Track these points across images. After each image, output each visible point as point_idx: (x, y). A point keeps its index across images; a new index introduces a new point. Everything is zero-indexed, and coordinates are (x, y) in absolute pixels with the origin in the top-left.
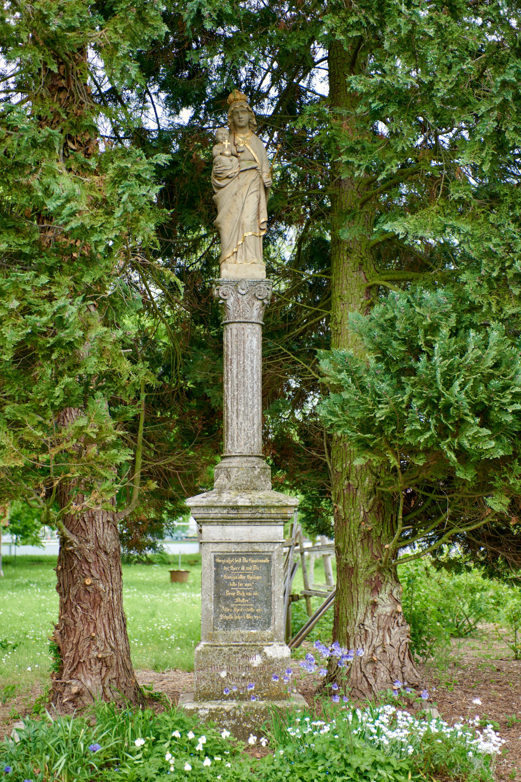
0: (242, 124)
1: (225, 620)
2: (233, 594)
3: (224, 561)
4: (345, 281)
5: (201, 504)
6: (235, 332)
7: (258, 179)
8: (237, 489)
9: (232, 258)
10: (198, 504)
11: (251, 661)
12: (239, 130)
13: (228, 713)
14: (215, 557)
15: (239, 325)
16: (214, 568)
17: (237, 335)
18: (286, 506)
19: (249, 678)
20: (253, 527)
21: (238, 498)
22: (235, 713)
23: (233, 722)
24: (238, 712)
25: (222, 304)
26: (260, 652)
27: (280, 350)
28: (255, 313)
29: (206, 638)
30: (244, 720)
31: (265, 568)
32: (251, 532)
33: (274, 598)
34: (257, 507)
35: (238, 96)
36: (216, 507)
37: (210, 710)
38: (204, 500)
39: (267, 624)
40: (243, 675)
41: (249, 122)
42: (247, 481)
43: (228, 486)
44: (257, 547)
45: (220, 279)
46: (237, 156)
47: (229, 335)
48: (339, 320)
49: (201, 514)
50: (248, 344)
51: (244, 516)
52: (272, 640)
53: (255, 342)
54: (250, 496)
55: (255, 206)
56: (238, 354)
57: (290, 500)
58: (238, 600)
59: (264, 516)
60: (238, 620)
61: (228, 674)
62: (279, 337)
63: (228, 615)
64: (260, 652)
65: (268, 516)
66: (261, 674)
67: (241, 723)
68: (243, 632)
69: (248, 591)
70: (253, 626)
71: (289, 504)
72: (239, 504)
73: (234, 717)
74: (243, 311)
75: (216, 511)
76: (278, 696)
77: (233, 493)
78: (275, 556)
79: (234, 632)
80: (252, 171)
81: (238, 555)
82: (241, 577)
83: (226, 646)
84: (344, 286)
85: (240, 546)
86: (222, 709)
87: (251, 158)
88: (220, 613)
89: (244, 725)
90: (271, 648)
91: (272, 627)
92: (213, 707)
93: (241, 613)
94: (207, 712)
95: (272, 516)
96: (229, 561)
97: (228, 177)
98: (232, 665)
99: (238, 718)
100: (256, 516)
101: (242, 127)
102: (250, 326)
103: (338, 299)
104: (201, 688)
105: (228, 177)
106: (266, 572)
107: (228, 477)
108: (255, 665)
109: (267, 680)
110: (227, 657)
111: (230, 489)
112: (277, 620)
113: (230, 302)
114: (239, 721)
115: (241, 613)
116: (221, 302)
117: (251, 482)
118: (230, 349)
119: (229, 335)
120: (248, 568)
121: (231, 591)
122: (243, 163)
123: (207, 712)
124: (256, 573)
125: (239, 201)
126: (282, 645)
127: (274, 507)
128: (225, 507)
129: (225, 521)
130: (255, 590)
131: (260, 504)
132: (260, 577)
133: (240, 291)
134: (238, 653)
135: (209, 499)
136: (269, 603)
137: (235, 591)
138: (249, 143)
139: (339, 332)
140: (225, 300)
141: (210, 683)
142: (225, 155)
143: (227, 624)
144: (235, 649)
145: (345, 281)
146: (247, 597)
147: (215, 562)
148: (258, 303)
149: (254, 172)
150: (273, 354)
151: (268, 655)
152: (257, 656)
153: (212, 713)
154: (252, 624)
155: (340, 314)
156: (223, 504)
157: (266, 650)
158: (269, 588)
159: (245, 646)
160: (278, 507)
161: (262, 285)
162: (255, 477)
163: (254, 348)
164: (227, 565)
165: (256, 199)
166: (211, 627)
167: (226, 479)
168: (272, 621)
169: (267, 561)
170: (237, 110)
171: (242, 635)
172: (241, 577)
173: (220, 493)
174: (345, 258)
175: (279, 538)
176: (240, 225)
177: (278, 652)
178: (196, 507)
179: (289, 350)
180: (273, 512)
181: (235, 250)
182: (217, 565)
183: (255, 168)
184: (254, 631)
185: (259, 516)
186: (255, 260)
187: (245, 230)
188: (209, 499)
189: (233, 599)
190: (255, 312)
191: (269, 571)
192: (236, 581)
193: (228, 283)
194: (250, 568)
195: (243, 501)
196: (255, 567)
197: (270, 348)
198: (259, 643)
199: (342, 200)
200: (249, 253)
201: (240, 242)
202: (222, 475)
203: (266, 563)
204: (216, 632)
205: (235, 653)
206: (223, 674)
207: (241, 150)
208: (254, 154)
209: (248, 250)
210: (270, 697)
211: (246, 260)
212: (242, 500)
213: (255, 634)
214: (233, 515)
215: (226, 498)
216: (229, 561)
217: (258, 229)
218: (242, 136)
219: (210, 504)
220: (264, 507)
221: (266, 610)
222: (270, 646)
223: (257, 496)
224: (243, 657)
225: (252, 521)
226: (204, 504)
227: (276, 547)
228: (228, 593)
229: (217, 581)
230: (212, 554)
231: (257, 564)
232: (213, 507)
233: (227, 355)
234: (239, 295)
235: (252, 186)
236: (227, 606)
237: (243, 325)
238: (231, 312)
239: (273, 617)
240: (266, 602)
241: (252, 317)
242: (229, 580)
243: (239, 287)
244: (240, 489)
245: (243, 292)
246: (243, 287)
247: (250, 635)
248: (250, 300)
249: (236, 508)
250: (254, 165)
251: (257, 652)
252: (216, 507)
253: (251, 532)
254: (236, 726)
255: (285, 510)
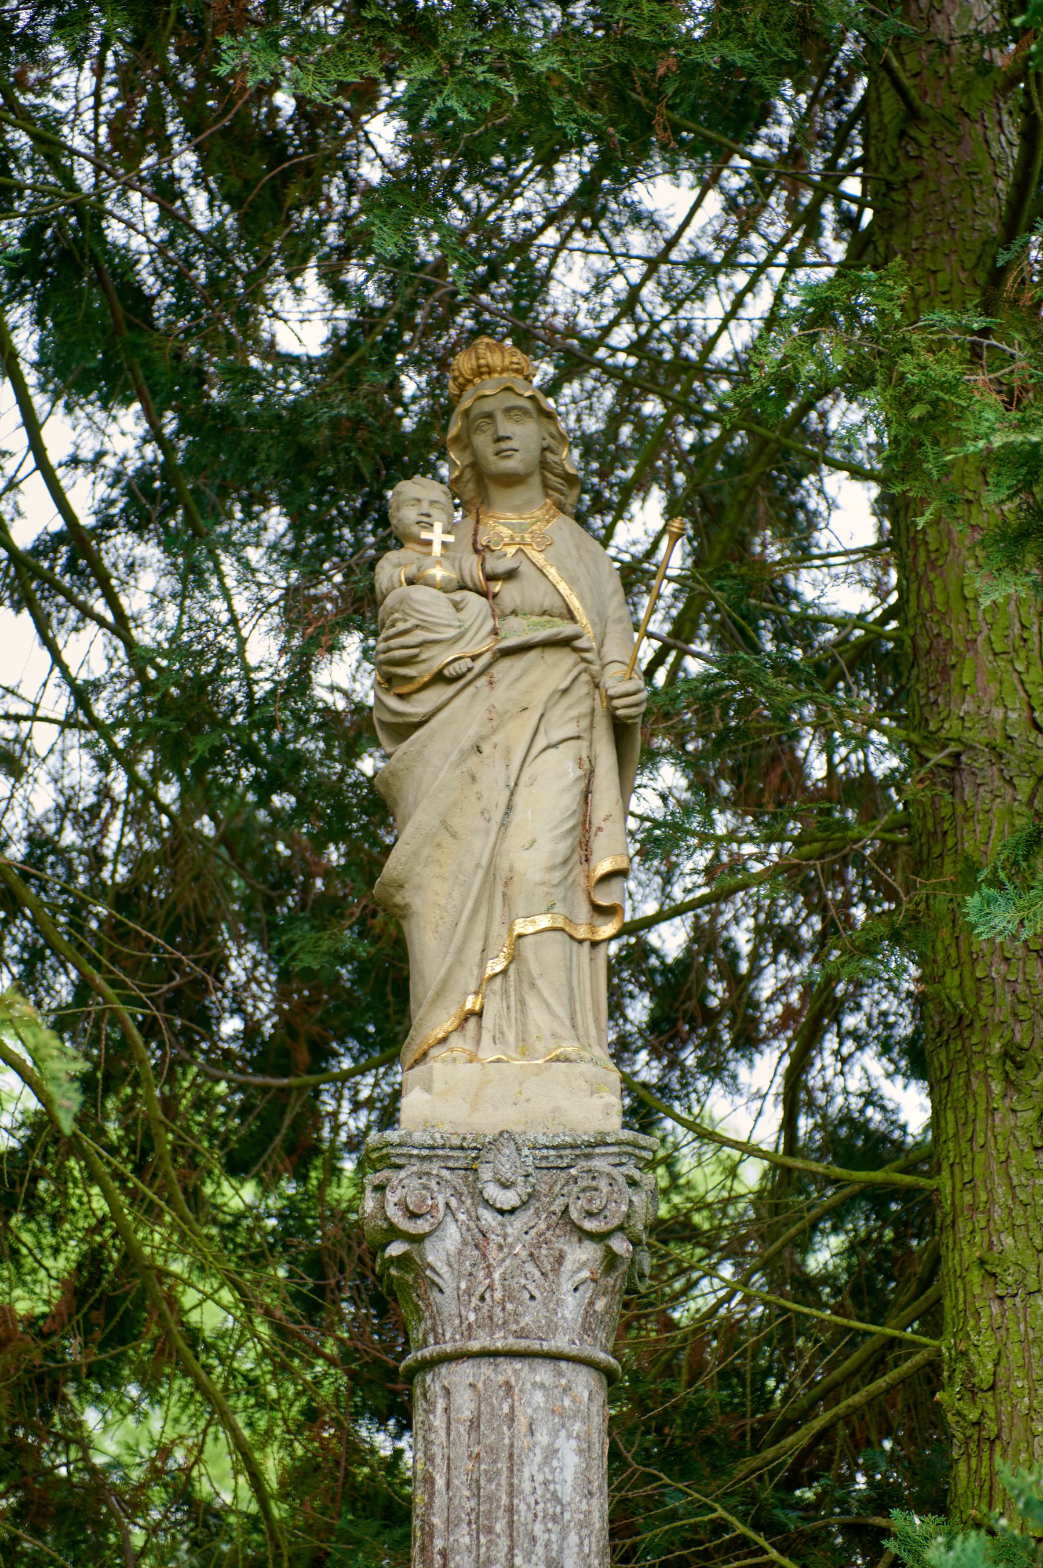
0: (512, 464)
4: (1001, 1192)
6: (465, 1404)
7: (582, 689)
9: (455, 1041)
12: (497, 495)
15: (486, 1368)
17: (474, 1424)
25: (404, 1261)
27: (720, 1527)
28: (571, 1307)
35: (495, 359)
41: (544, 465)
45: (392, 1135)
46: (484, 594)
47: (438, 1421)
48: (984, 1374)
50: (531, 1468)
53: (570, 1461)
55: (570, 800)
56: (481, 1527)
62: (717, 1470)
74: (509, 1296)
80: (553, 655)
84: (998, 1214)
87: (550, 602)
97: (440, 678)
101: (511, 480)
102: (543, 1373)
103: (975, 1276)
105: (440, 678)
113: (442, 1252)
116: (396, 1249)
118: (440, 1501)
119: (438, 1421)
122: (513, 621)
125: (493, 777)
133: (492, 1191)
138: (546, 545)
139: (991, 1428)
140: (417, 1239)
142: (430, 583)
145: (1001, 1192)
148: (581, 1257)
149: (564, 662)
150: (686, 1544)
155: (987, 1343)
161: (600, 1164)
163: (567, 1492)
165: (573, 772)
170: (487, 406)
174: (997, 1088)
176: (496, 883)
179: (756, 1527)
181: (471, 1003)
183: (566, 643)
186: (569, 1048)
187: (520, 907)
190: (569, 1302)
193: (431, 1152)
197: (673, 1516)
199: (968, 846)
200: (537, 1015)
201: (496, 966)
207: (501, 566)
208: (563, 587)
209: (532, 1002)
211: (524, 1047)
217: (584, 911)
218: (513, 518)
233: (429, 1534)
234: (488, 1217)
235: (556, 714)
237: (509, 1369)
238: (446, 1302)
241: (552, 1328)
243: (486, 1173)
245: (508, 1199)
246: (506, 1171)
248: (542, 1240)
250: (567, 629)
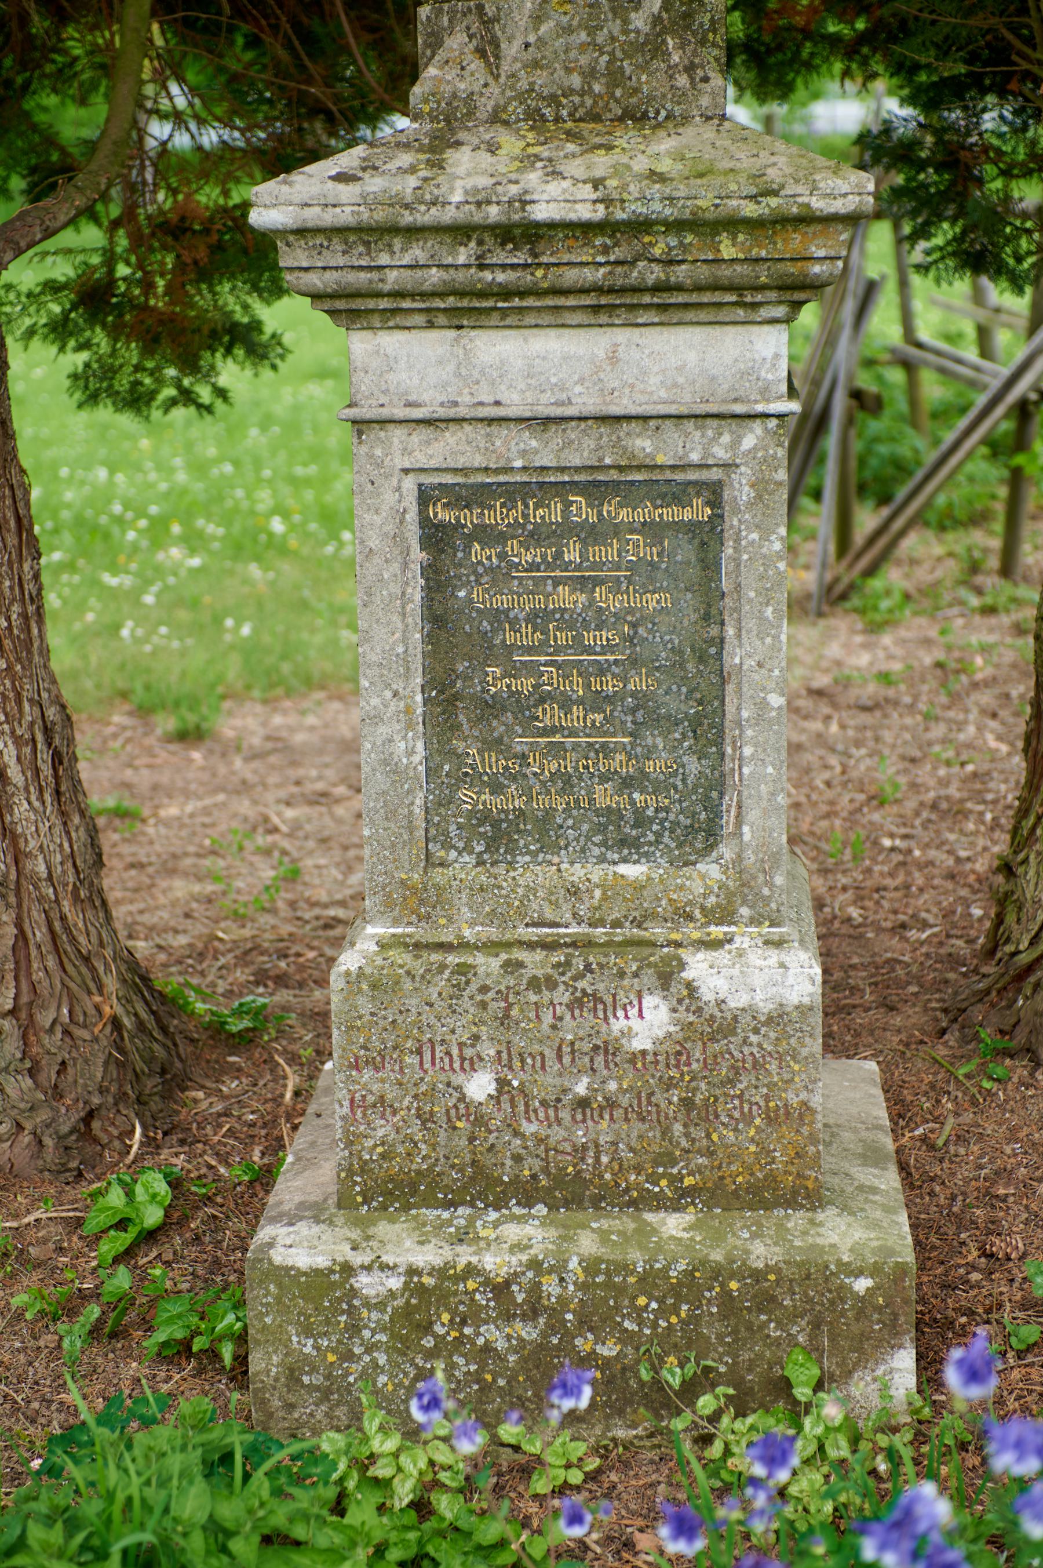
1: (485, 817)
2: (526, 685)
3: (469, 518)
5: (329, 218)
8: (535, 118)
10: (313, 216)
11: (618, 1025)
13: (501, 1289)
14: (425, 497)
16: (418, 556)
18: (806, 219)
19: (611, 1104)
20: (622, 336)
21: (533, 177)
22: (536, 1287)
23: (528, 1332)
24: (550, 1286)
26: (667, 976)
29: (389, 904)
30: (585, 1323)
31: (686, 552)
32: (613, 359)
33: (740, 708)
34: (640, 226)
36: (414, 232)
37: (412, 1271)
38: (346, 192)
39: (703, 832)
40: (581, 1089)
42: (590, 74)
43: (485, 106)
44: (643, 444)
49: (336, 265)
51: (571, 276)
52: (725, 915)
54: (601, 163)
57: (829, 182)
58: (549, 715)
59: (681, 273)
60: (549, 813)
61: (502, 1083)
63: (497, 788)
64: (667, 976)
65: (703, 273)
66: (669, 1085)
67: (568, 1336)
68: (577, 872)
69: (602, 670)
70: (629, 847)
71: (818, 204)
72: (541, 213)
73: (533, 1310)
75: (417, 253)
76: (755, 1190)
77: (510, 144)
78: (741, 490)
79: (532, 875)
81: (542, 487)
82: (566, 597)
83: (492, 947)
85: (555, 437)
86: (470, 1271)
88: (461, 779)
89: (584, 1344)
90: (721, 956)
91: (726, 851)
92: (428, 1256)
93: (566, 782)
94: (395, 1283)
95: (725, 272)
96: (495, 516)
98: (519, 1043)
99: (555, 1313)
100: (634, 268)
104: (369, 1148)
106: (693, 572)
107: (488, 50)
108: (638, 1044)
109: (698, 1112)
110: (497, 1007)
111: (496, 118)
112: (753, 815)
114: (556, 1324)
115: (566, 782)
117: (615, 77)
120: (596, 553)
121: (513, 671)
123: (395, 1283)
124: (643, 575)
126: (778, 944)
127: (733, 224)
128: (460, 232)
129: (466, 307)
130: (634, 662)
131: (657, 208)
132: (665, 600)
134: (551, 984)
135: (374, 184)
136: (708, 729)
137: (532, 669)
141: (415, 1129)
143: (498, 837)
144: (535, 962)
146: (597, 701)
147: (425, 522)
151: (707, 994)
152: (649, 1001)
153: (422, 1290)
154: (624, 836)
156: (448, 215)
157: (698, 966)
158: (710, 653)
159: (589, 944)
160: (755, 225)
162: (633, 49)
164: (484, 534)
166: (417, 850)
167: (476, 65)
168: (728, 820)
169: (697, 511)
171: (574, 891)
172: (566, 597)
173: (438, 146)
175: (765, 394)
177: (758, 980)
178: (301, 232)
180: (727, 250)
182: (436, 538)
184: (631, 871)
185: (655, 274)
188: (374, 184)
189: (523, 708)
191: (710, 565)
192: (538, 619)
194: (612, 554)
195: (557, 196)
196: (639, 548)
198: (657, 931)
202: (456, 42)
203: (692, 528)
204: (439, 876)
205: (534, 984)
206: (480, 1086)
210: (716, 1196)
212: (555, 188)
213: (639, 887)
214: (514, 268)
215: (472, 176)
216: (495, 516)
219: (380, 216)
220: (678, 226)
221: (693, 766)
222: (715, 944)
223: (641, 164)
224: (576, 1004)
225: (613, 303)
226: (345, 216)
227: (749, 442)
228: (496, 680)
229: (439, 618)
230: (409, 484)
231: (645, 528)
232: (393, 230)
236: (496, 745)
239: (730, 800)
240: (695, 723)
242: (499, 616)
244: (560, 117)
247: (613, 889)
249: (525, 235)
251: (649, 977)
252: (414, 232)
253: (613, 359)
254: (542, 1347)
255: (794, 242)
